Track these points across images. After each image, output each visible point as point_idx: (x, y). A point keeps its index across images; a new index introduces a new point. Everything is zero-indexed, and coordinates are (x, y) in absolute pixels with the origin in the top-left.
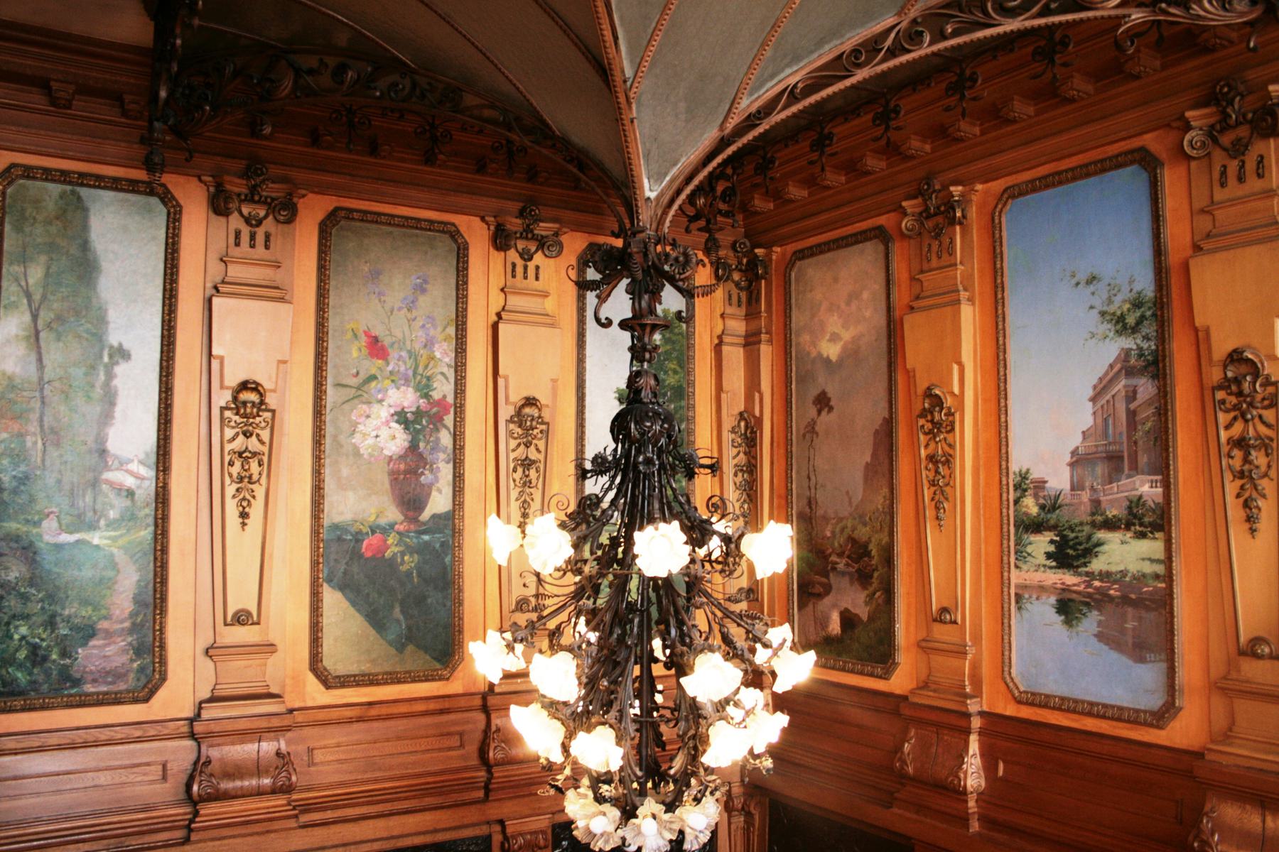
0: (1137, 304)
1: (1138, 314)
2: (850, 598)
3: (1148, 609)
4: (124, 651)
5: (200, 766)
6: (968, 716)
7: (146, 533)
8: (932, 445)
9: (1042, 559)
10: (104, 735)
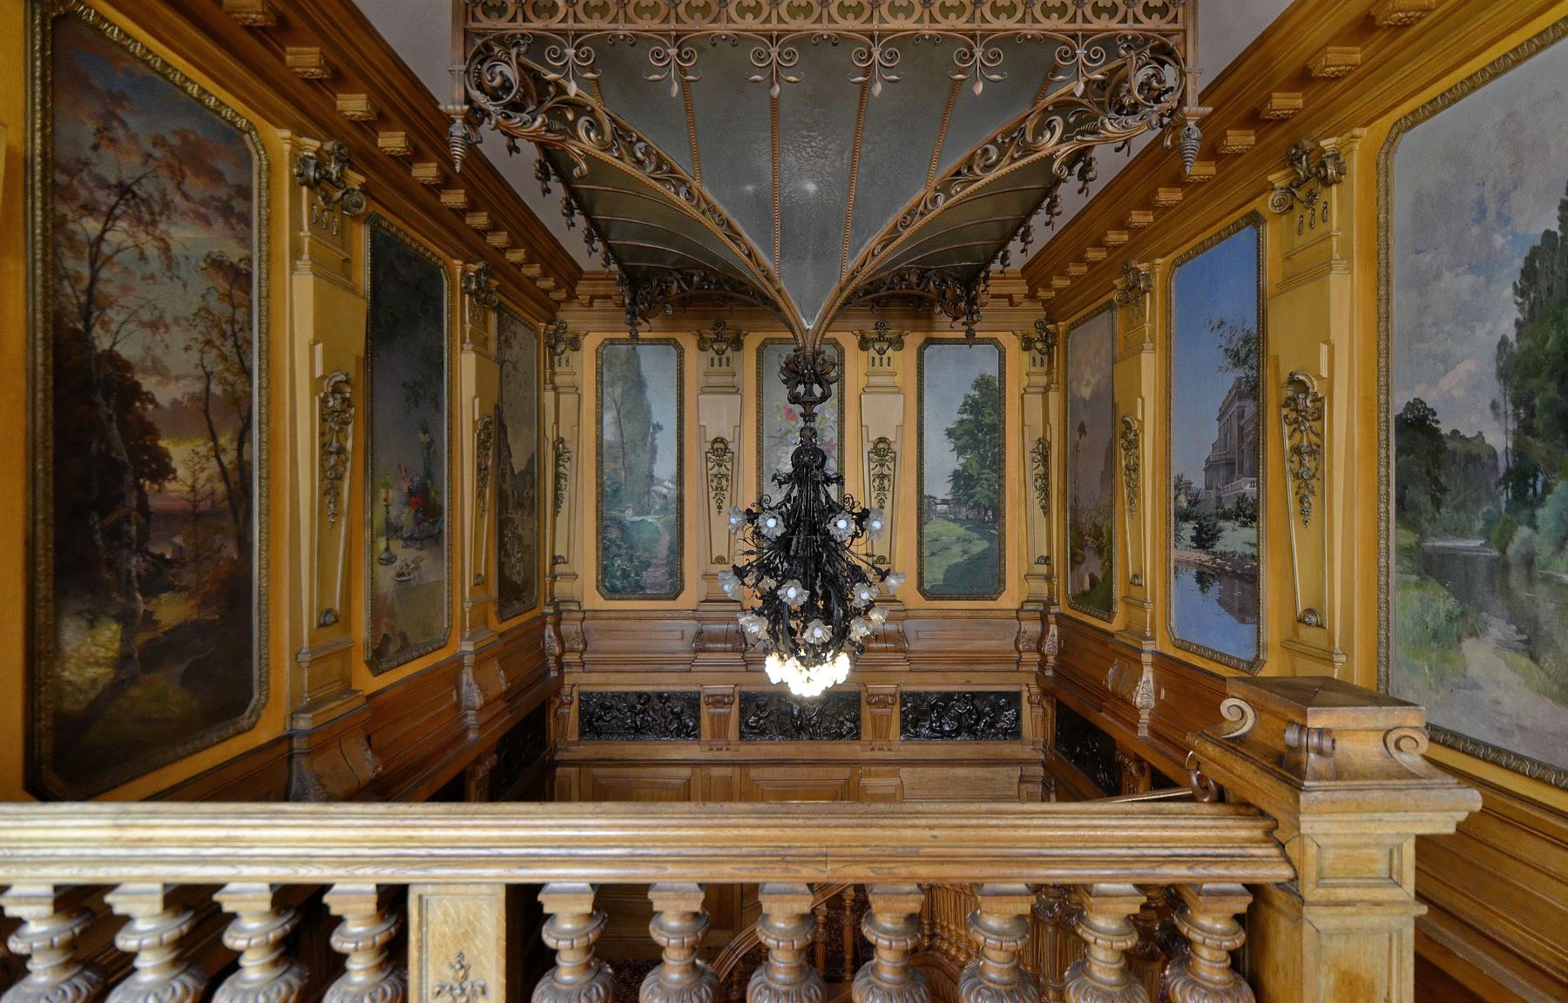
5: (700, 634)
6: (1141, 651)
7: (673, 517)
9: (1188, 541)
10: (661, 614)
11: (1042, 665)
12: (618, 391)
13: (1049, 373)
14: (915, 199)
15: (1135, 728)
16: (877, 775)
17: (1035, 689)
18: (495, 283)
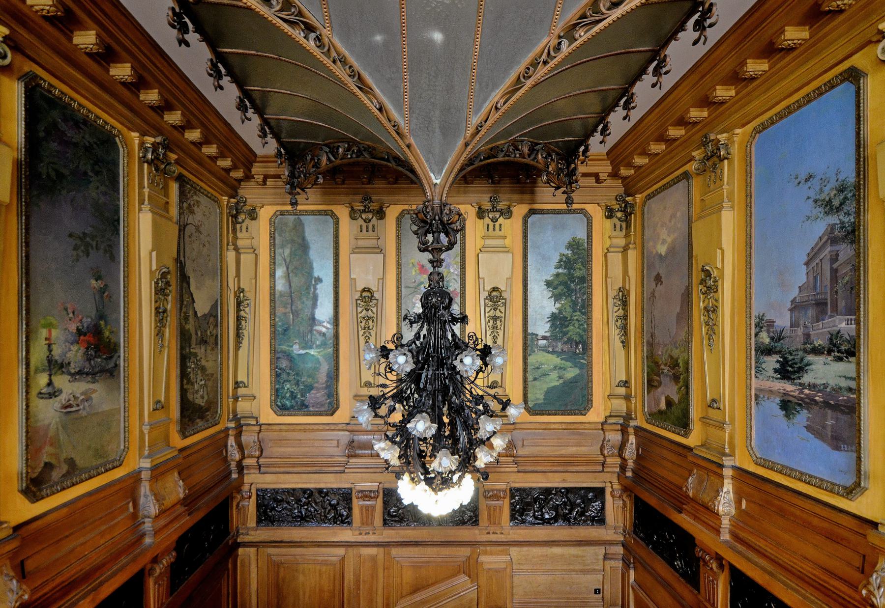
0: (841, 190)
1: (842, 197)
2: (670, 390)
3: (843, 412)
4: (323, 395)
6: (721, 466)
7: (330, 350)
8: (707, 301)
9: (771, 373)
11: (623, 468)
12: (287, 252)
13: (627, 236)
14: (537, 49)
15: (717, 531)
16: (491, 554)
17: (616, 486)
18: (173, 157)
